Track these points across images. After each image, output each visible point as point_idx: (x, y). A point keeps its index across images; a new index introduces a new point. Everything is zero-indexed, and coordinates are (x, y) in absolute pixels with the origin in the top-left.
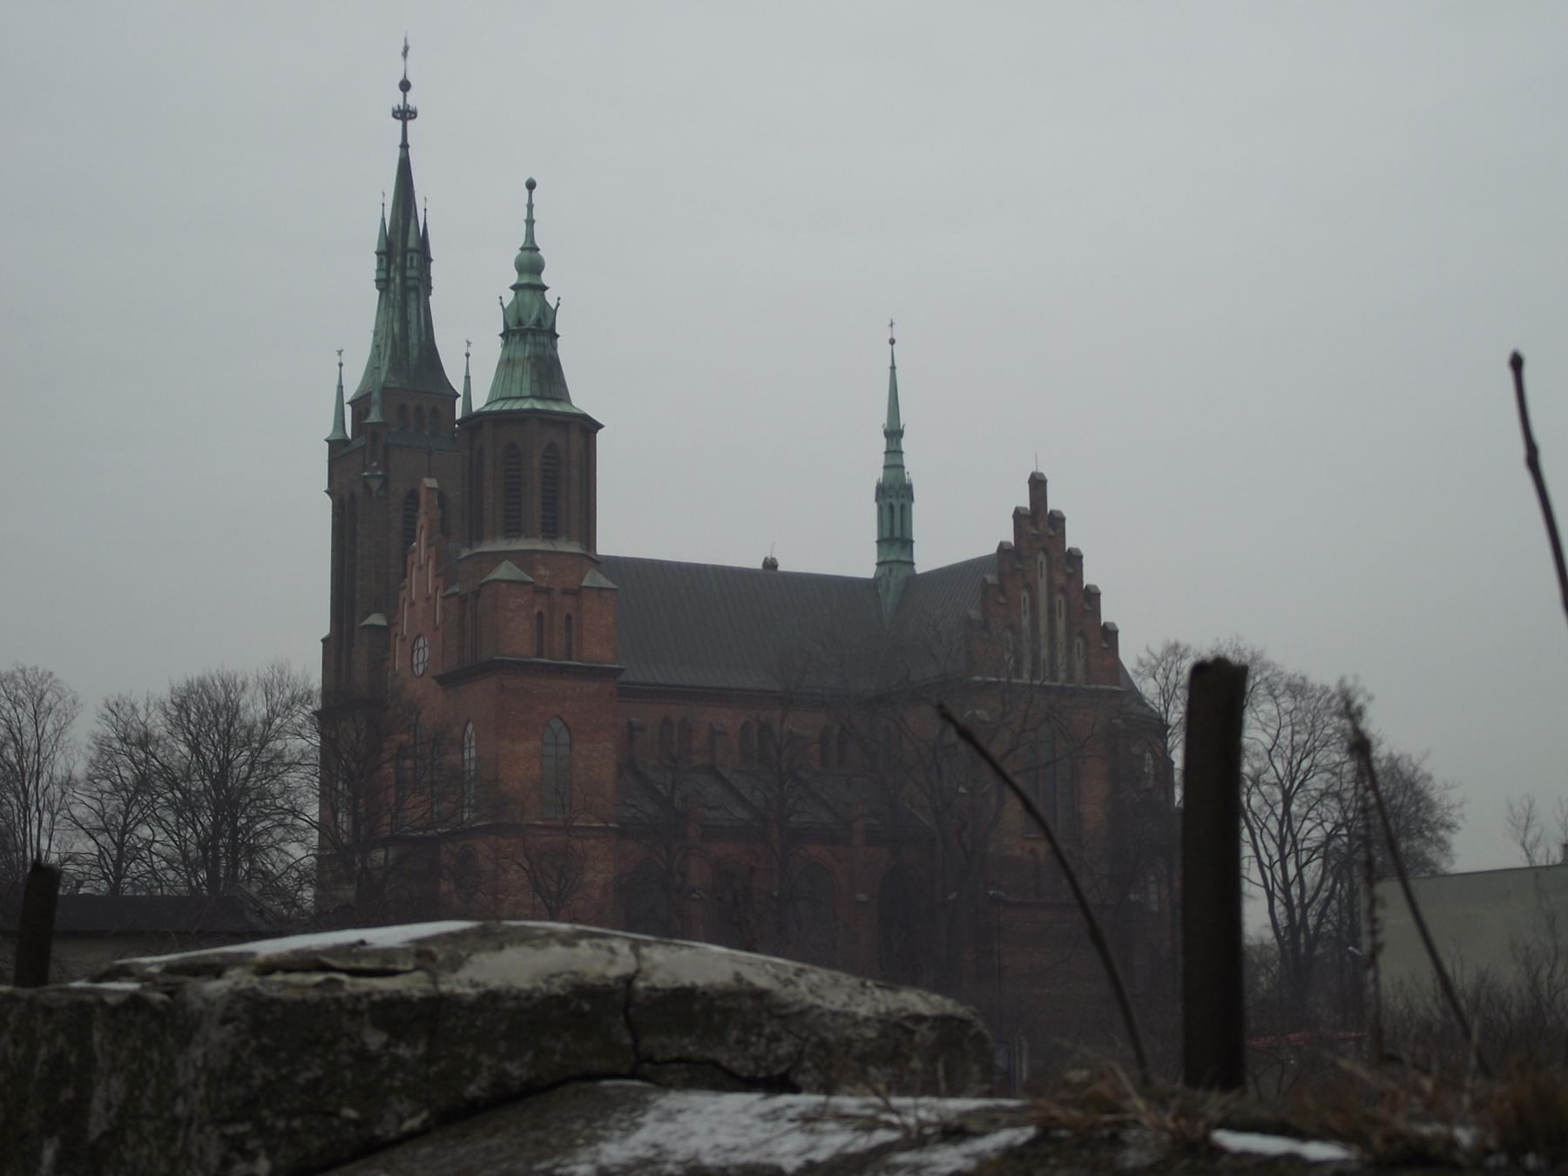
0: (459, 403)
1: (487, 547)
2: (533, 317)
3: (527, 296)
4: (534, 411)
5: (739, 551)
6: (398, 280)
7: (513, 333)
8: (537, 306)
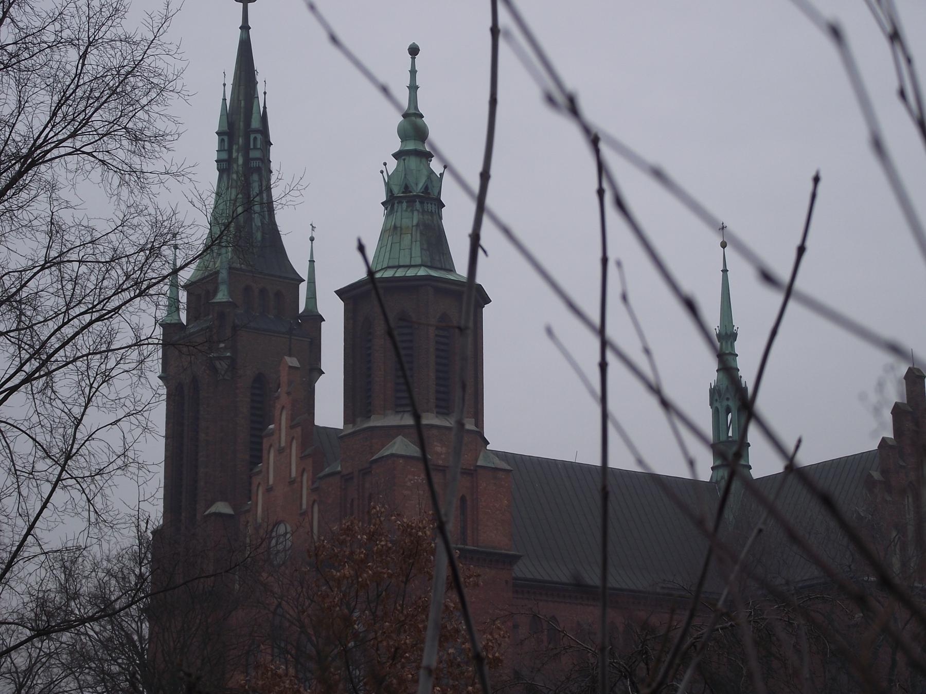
0: (303, 288)
1: (376, 422)
2: (421, 185)
3: (413, 162)
4: (429, 278)
5: (569, 457)
6: (241, 161)
7: (400, 200)
8: (425, 172)
